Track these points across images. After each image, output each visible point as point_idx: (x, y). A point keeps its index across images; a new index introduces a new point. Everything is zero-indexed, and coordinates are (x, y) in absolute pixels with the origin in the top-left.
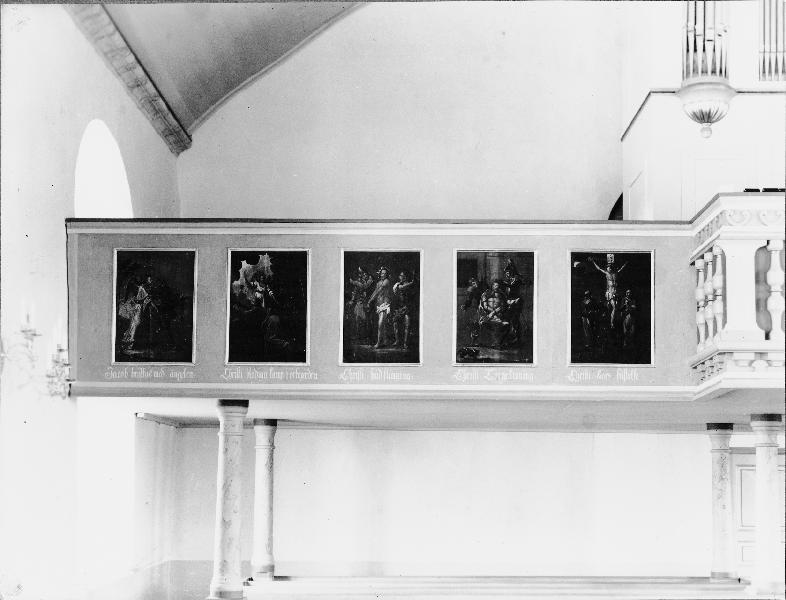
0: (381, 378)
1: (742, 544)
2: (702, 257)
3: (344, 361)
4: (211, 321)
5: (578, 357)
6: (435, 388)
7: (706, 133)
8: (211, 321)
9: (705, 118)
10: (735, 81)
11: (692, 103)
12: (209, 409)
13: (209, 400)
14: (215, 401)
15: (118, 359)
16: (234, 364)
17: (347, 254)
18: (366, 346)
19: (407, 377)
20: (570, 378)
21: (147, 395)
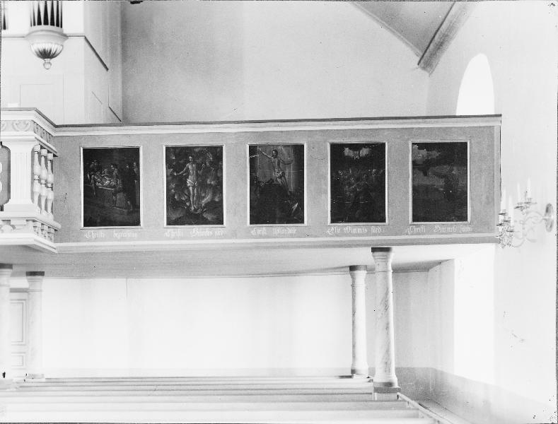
0: (197, 236)
1: (24, 343)
2: (49, 152)
3: (331, 223)
4: (236, 192)
5: (335, 219)
6: (146, 242)
7: (47, 66)
8: (236, 192)
9: (46, 55)
10: (67, 27)
11: (38, 43)
12: (363, 256)
13: (366, 248)
14: (370, 249)
15: (414, 220)
16: (333, 224)
17: (85, 150)
18: (296, 205)
19: (135, 235)
20: (167, 234)
21: (413, 244)
